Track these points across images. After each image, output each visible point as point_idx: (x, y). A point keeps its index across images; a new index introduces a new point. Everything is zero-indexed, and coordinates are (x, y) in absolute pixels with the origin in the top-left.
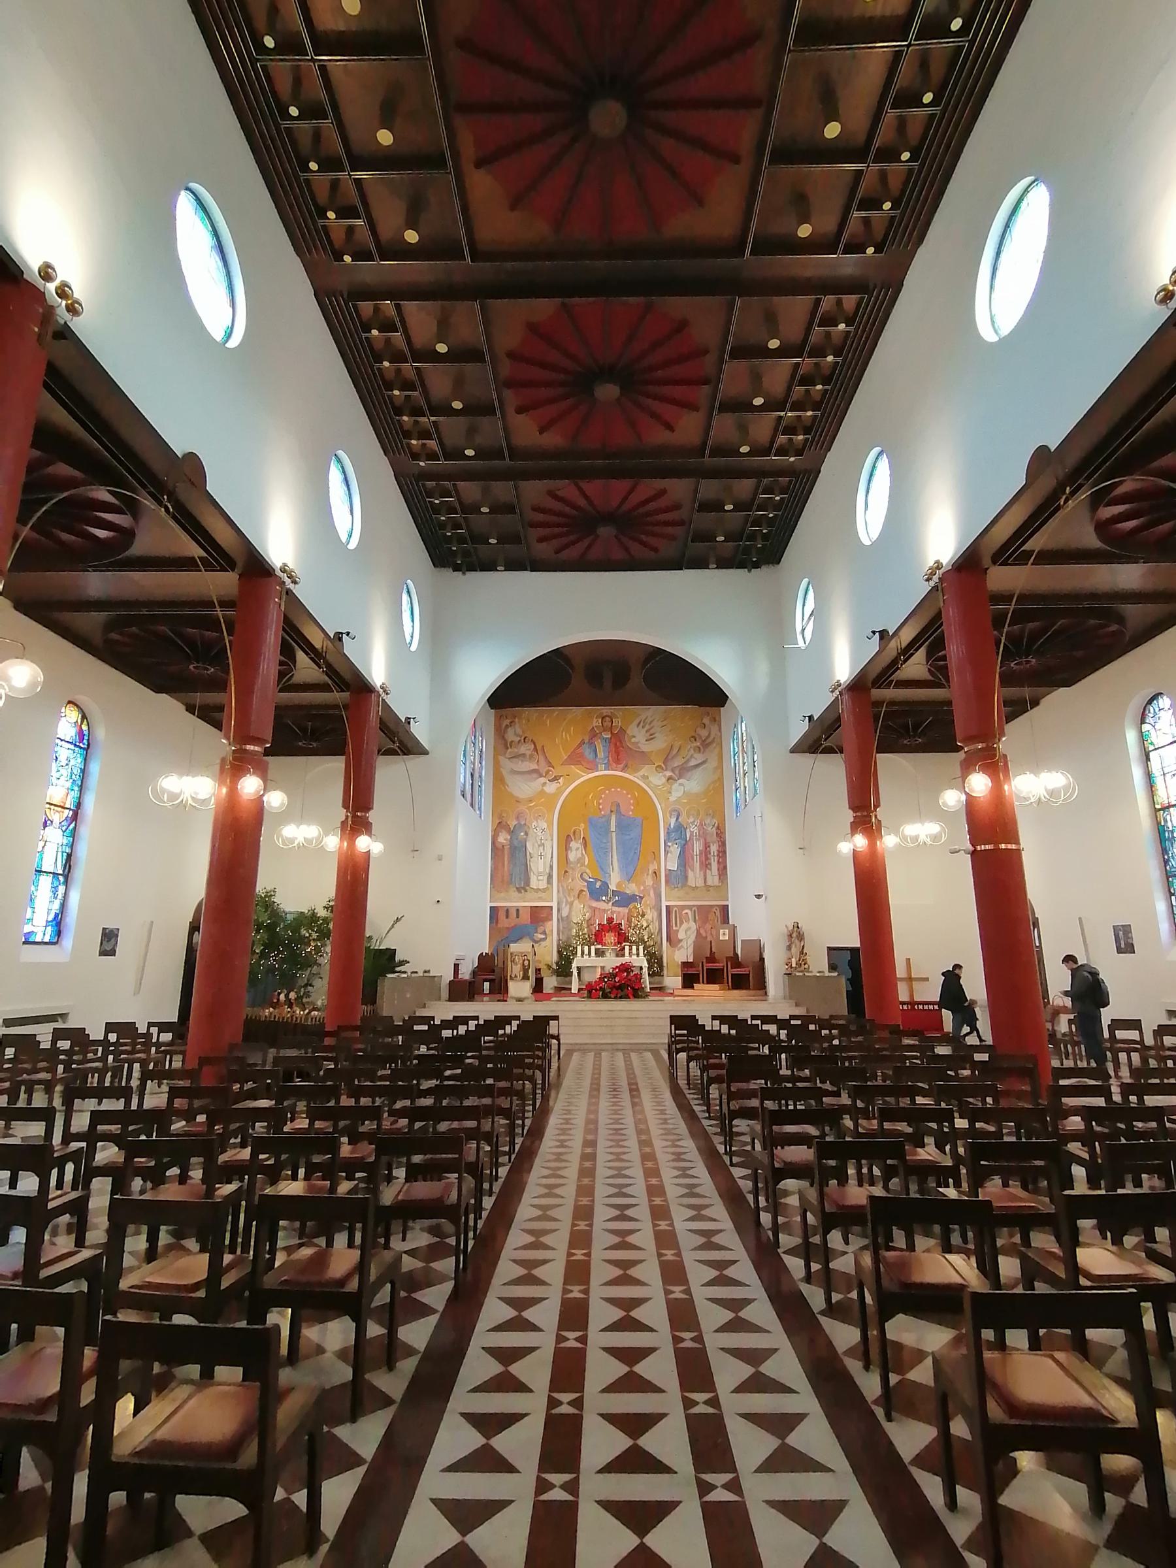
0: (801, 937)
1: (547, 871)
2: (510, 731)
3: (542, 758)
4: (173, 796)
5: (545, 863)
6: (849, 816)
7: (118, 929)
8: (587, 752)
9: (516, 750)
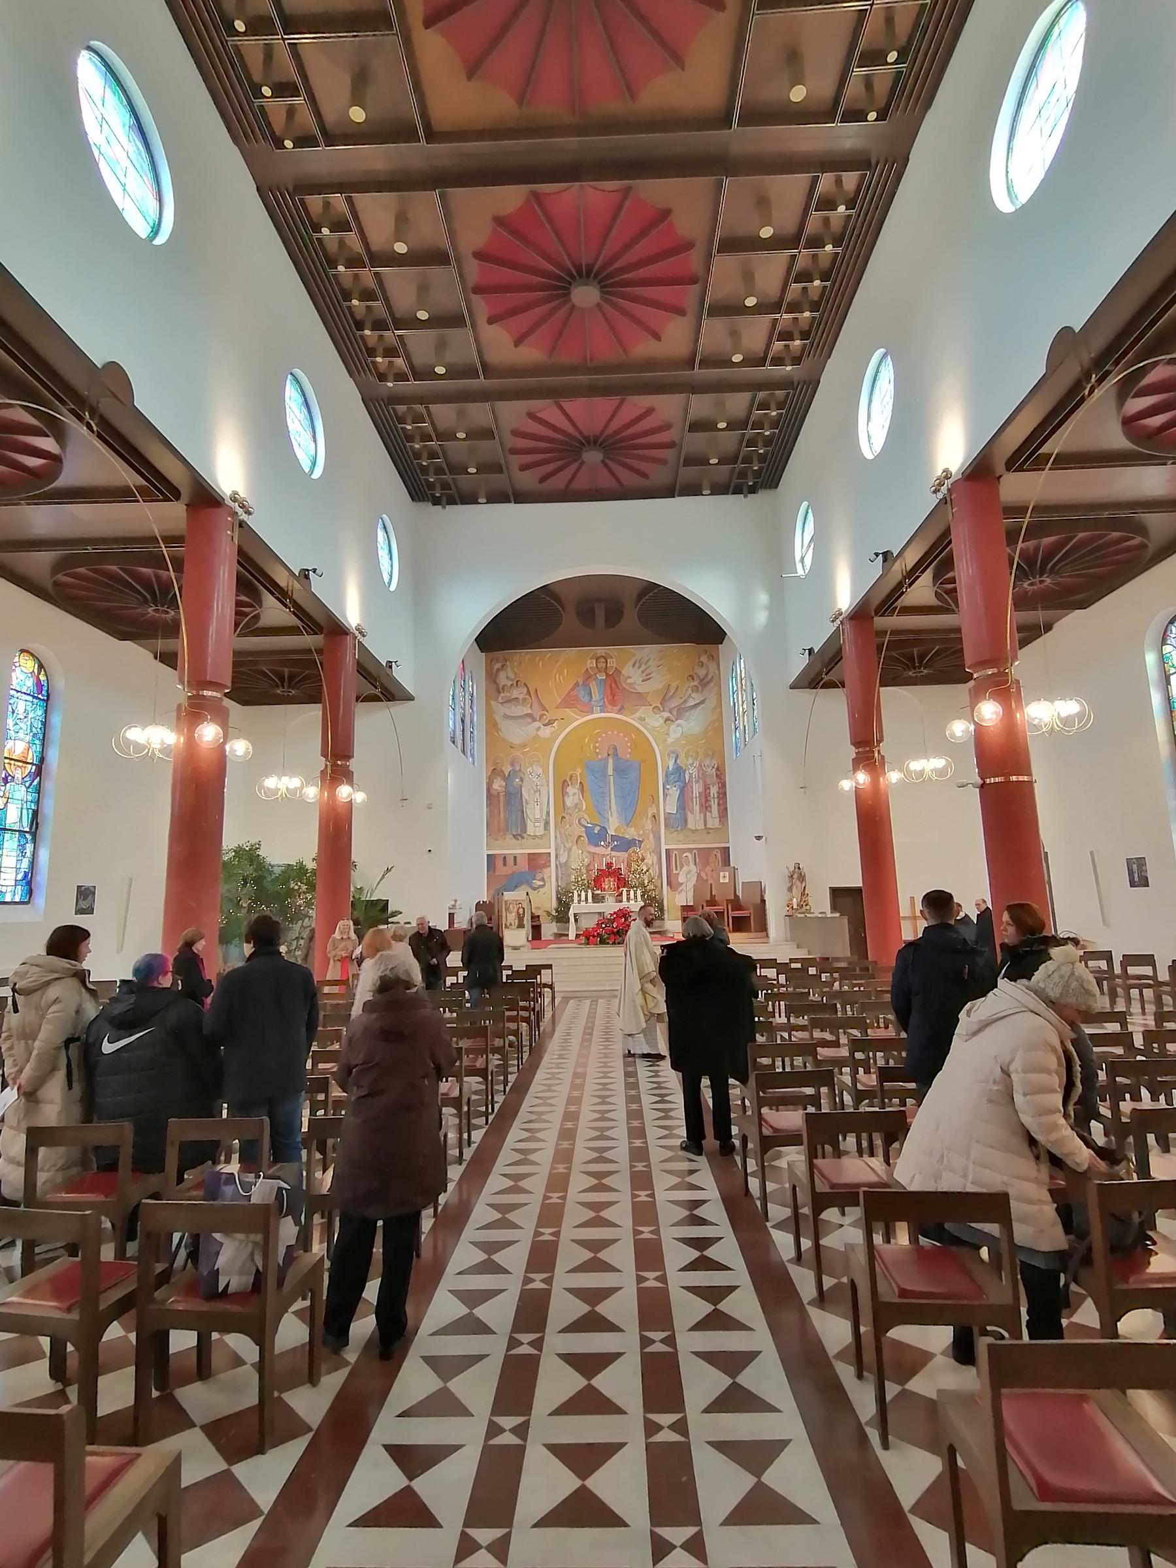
0: (802, 878)
2: (502, 675)
3: (535, 703)
4: (139, 747)
5: (541, 810)
6: (852, 752)
7: (95, 887)
8: (582, 694)
9: (508, 694)
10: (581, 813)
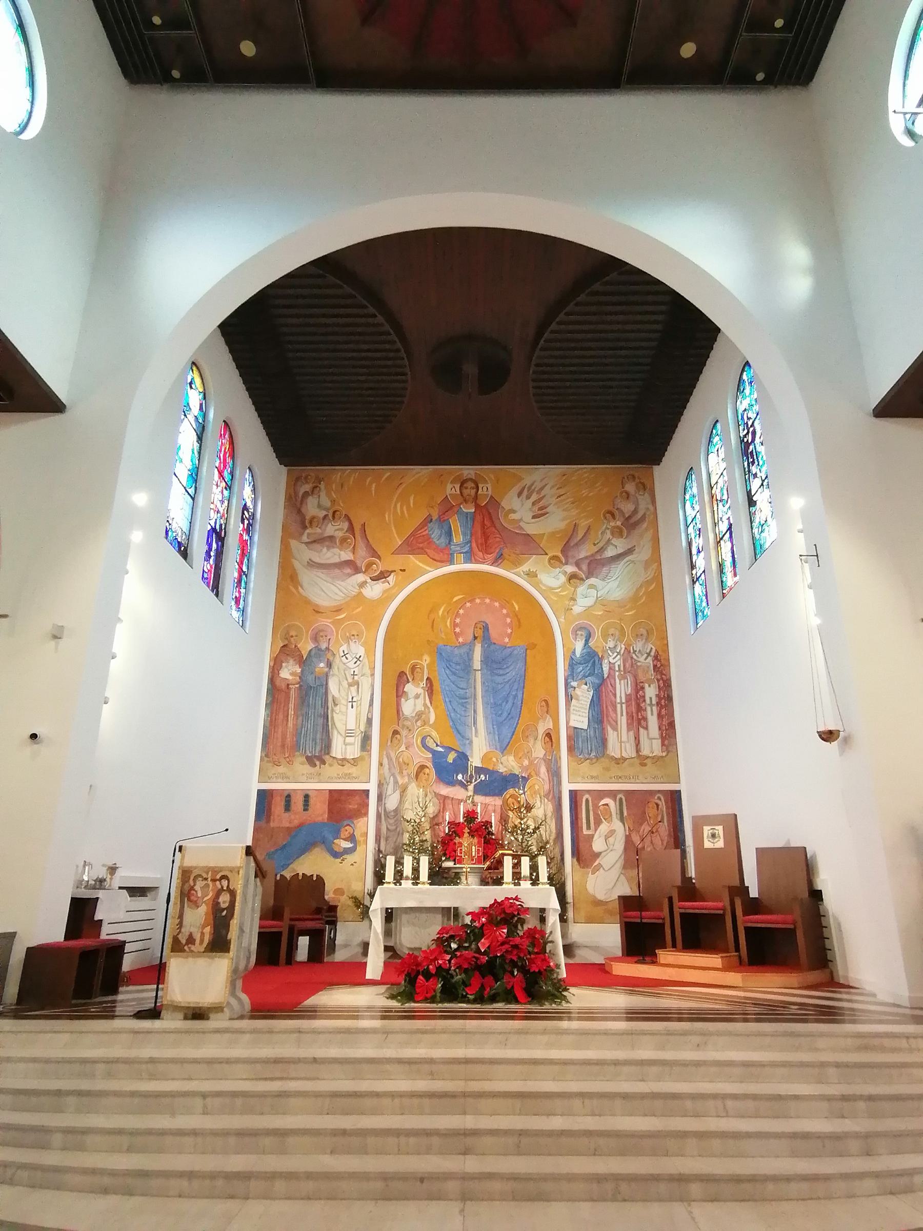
1: (362, 728)
8: (436, 534)
9: (319, 530)
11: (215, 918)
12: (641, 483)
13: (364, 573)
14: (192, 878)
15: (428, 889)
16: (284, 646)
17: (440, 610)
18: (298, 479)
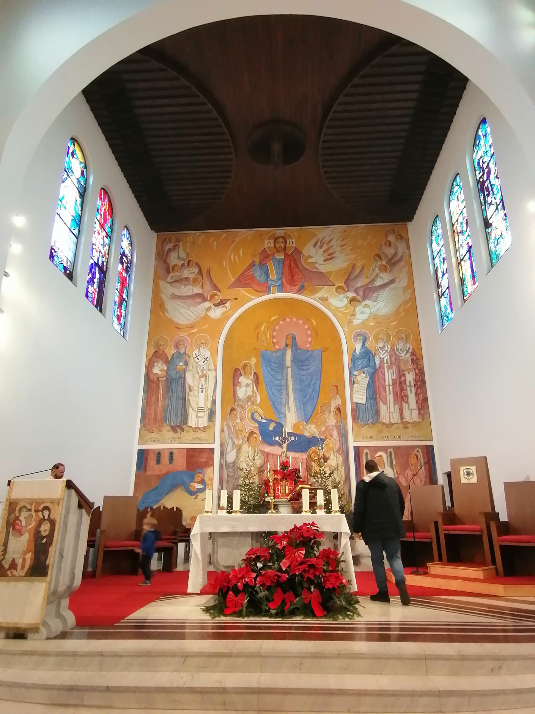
1: (209, 406)
8: (258, 274)
9: (178, 274)
10: (255, 407)
11: (36, 546)
12: (399, 235)
13: (209, 301)
14: (17, 509)
15: (239, 517)
16: (156, 351)
17: (262, 326)
18: (164, 241)
